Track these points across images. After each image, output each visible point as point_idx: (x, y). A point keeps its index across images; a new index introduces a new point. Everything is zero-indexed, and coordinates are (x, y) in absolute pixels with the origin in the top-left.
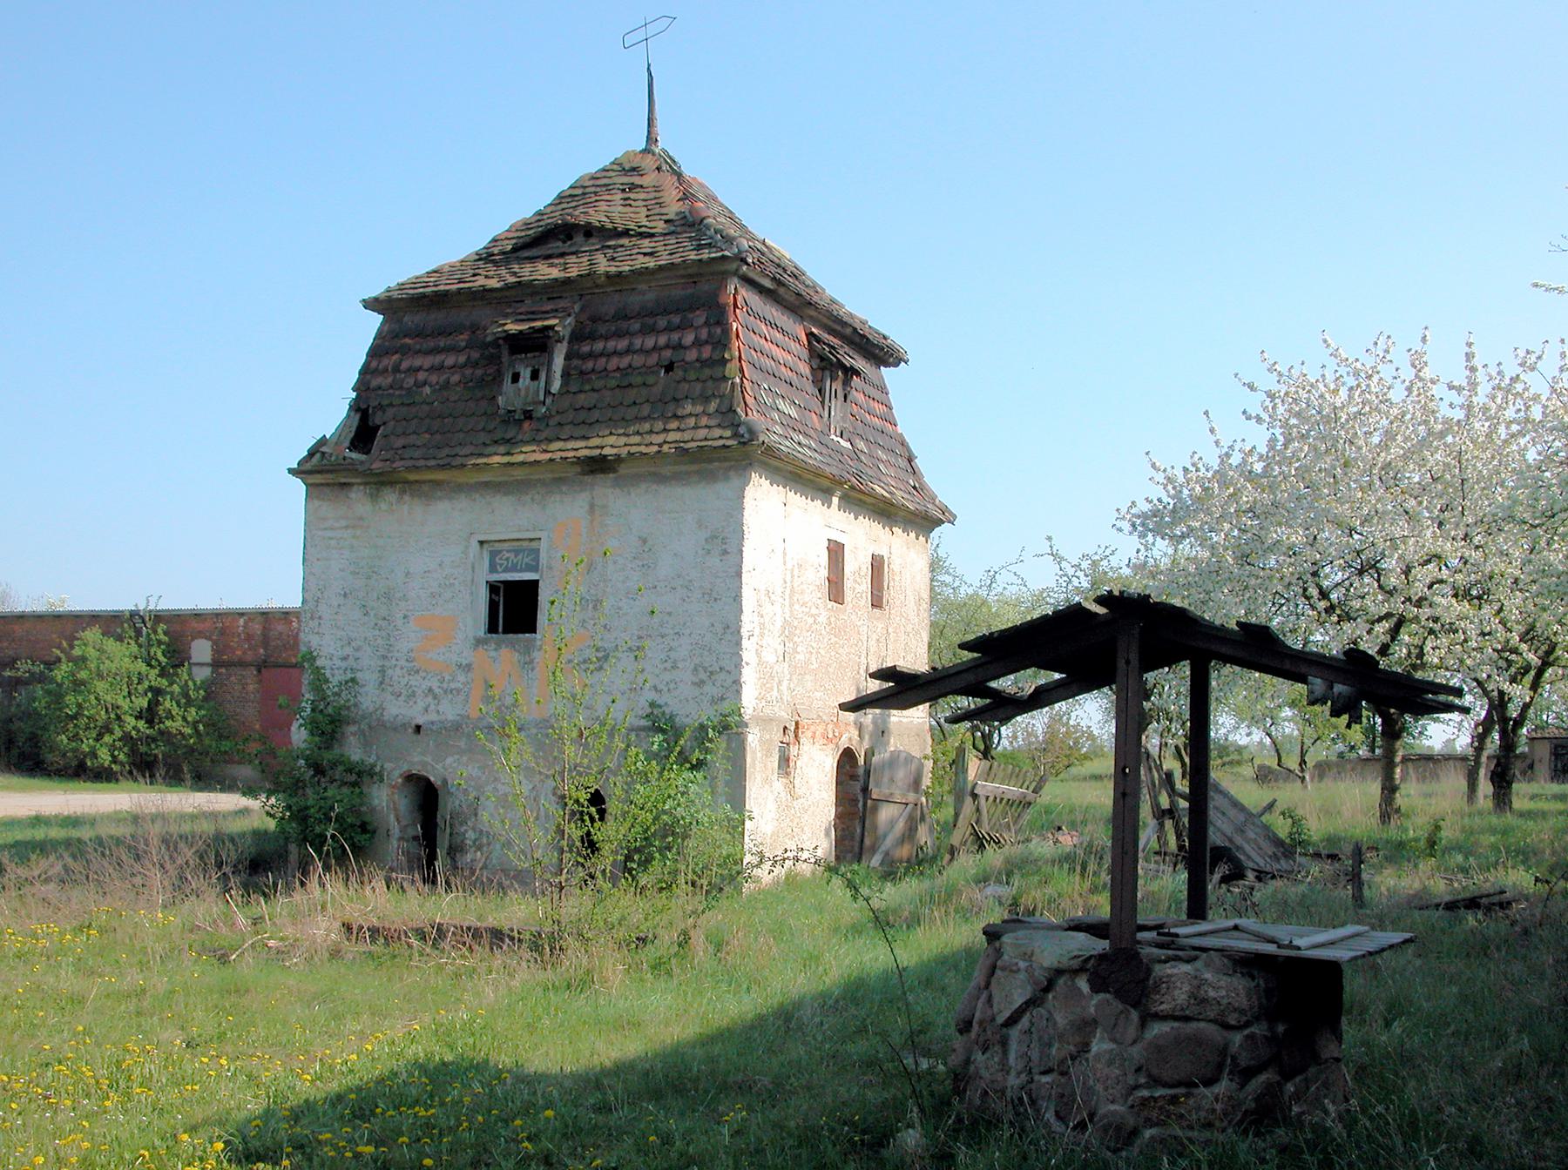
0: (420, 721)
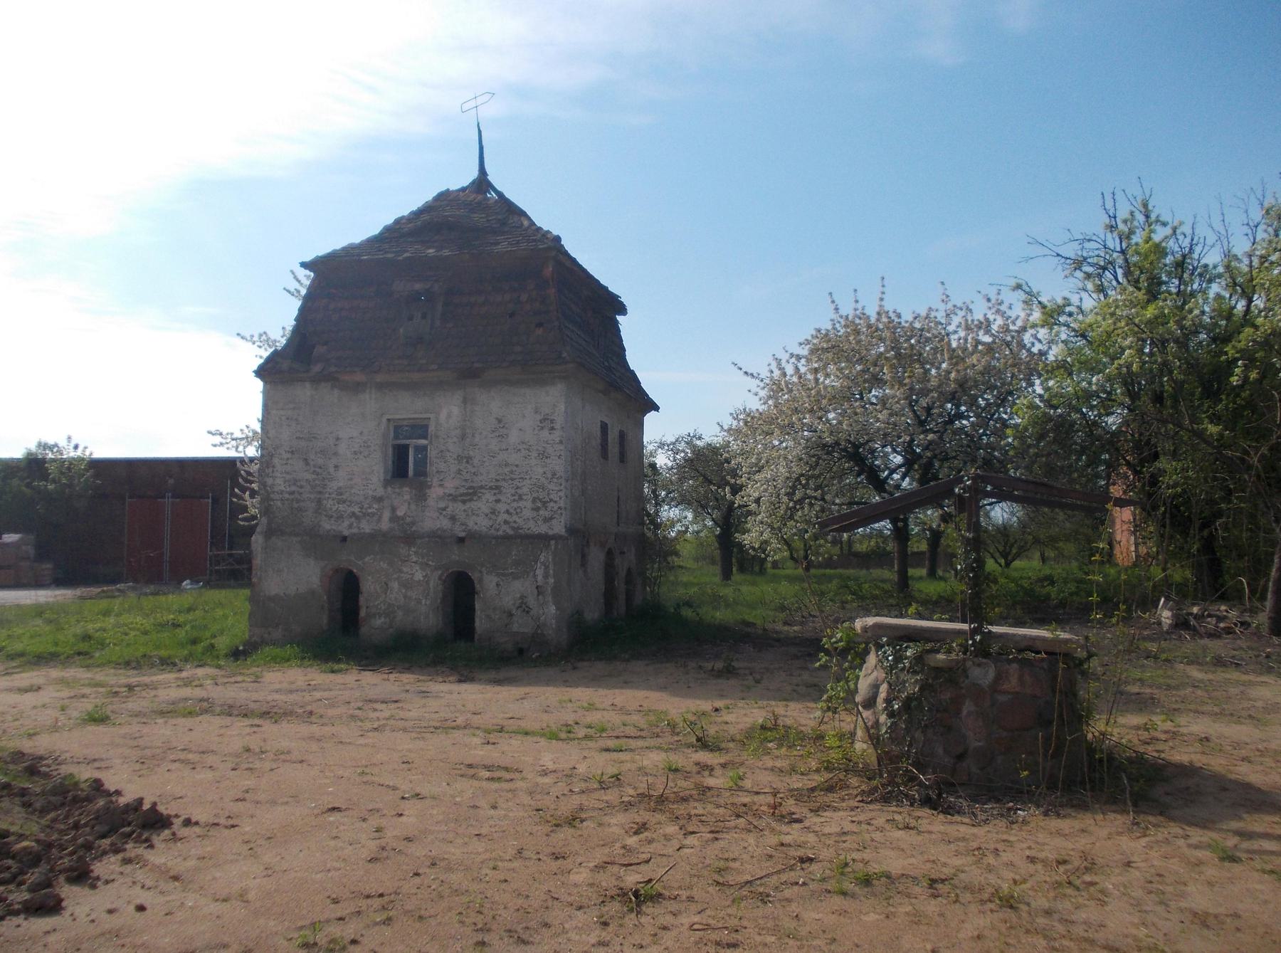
0: (346, 533)
